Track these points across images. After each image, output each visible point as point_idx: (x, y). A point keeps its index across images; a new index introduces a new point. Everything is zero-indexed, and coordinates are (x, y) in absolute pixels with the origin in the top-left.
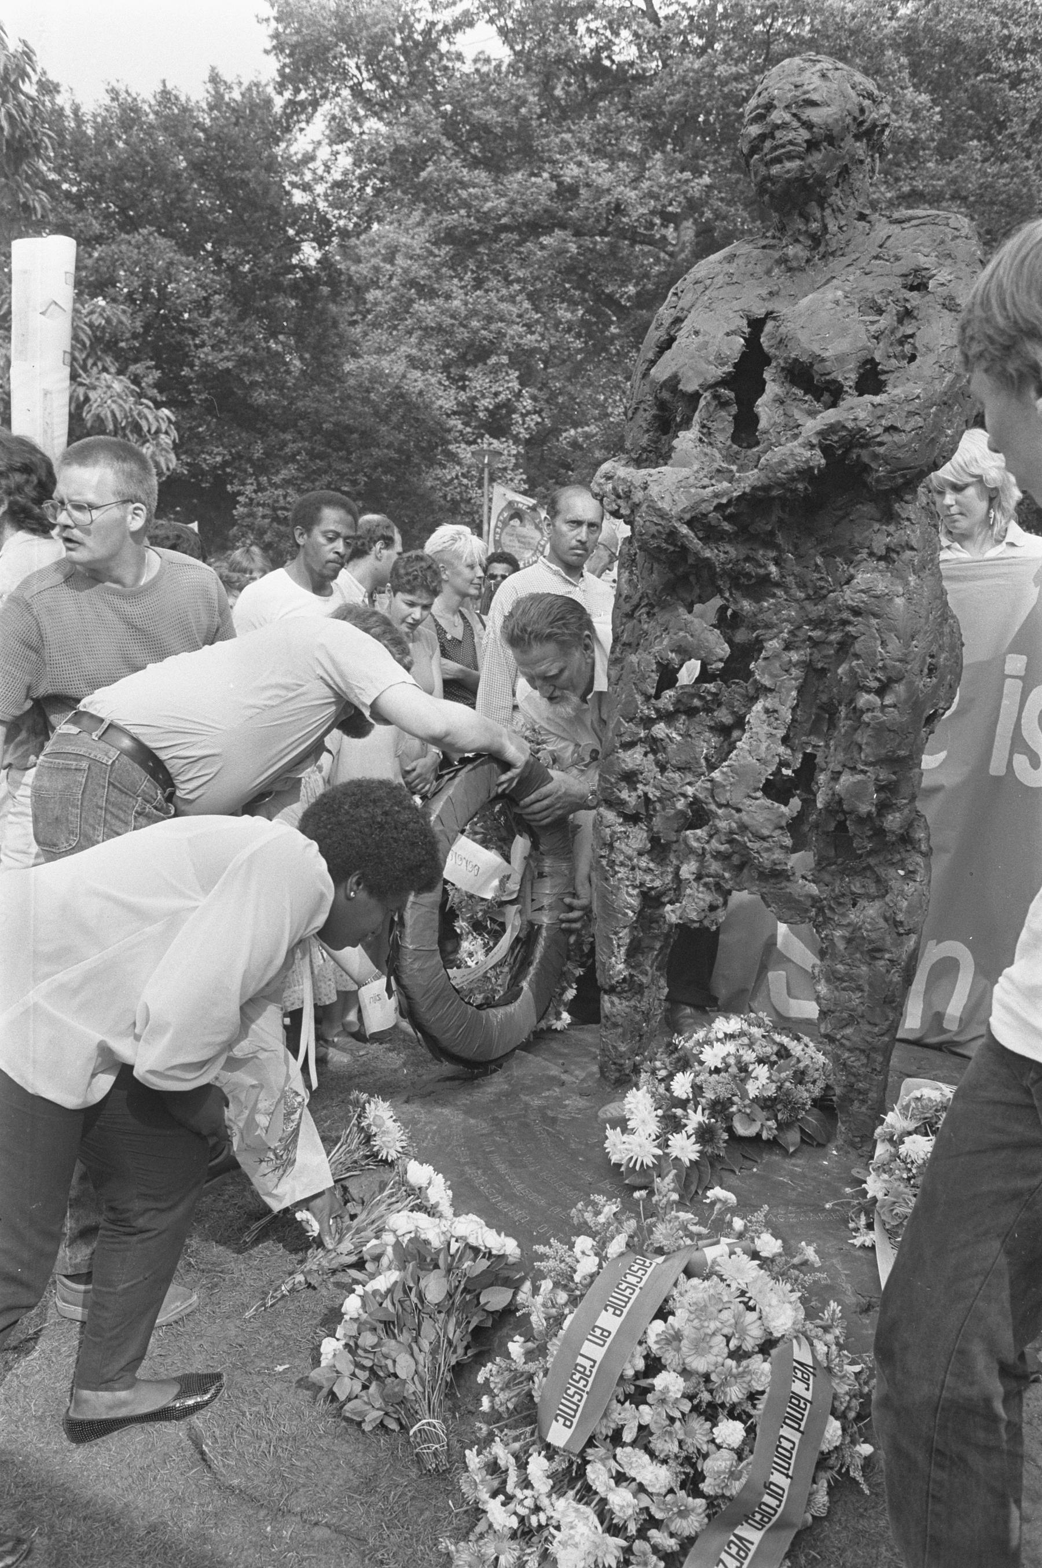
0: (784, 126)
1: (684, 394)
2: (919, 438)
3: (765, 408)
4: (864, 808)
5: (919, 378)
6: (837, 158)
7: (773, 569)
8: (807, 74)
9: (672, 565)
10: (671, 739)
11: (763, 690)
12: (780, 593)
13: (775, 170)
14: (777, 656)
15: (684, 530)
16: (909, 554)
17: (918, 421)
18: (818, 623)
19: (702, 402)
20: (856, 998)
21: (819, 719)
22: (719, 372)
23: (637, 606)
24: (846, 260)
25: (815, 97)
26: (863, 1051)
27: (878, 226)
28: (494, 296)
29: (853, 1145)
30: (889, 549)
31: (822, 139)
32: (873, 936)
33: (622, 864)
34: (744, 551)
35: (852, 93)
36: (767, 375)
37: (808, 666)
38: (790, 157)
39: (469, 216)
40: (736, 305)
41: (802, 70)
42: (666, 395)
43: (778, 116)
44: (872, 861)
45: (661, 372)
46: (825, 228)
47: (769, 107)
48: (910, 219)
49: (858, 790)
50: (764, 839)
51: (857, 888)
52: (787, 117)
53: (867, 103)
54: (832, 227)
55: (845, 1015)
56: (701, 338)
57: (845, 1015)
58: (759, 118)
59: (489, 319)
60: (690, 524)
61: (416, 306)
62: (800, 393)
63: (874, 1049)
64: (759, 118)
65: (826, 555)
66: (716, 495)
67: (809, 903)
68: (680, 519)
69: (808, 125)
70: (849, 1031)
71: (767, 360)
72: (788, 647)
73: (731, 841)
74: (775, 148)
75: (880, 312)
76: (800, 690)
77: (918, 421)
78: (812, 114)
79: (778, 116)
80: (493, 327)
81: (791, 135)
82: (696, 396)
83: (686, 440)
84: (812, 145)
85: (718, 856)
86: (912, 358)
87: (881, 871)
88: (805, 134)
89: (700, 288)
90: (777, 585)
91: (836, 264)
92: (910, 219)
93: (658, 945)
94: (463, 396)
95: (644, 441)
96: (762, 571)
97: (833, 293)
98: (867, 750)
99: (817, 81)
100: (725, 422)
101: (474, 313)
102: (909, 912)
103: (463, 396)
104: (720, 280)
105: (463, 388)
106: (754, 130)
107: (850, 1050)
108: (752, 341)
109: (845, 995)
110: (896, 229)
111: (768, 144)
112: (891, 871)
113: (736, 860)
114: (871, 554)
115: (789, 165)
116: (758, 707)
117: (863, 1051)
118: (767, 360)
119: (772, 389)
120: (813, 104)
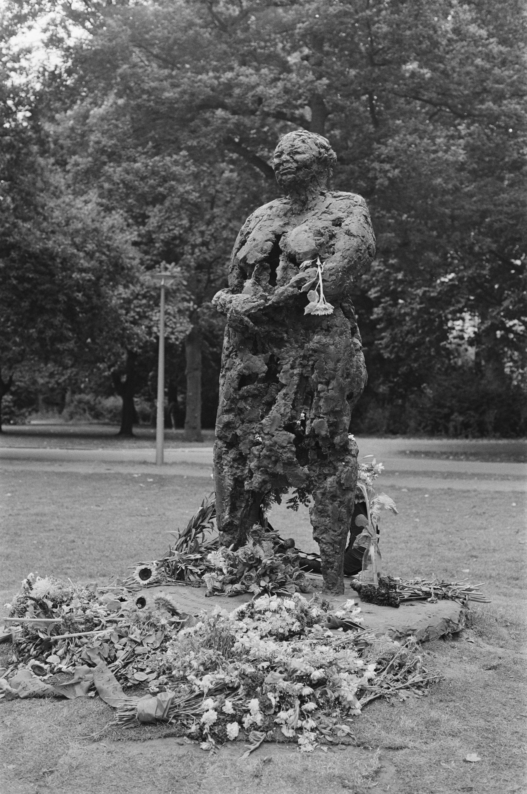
0: (287, 161)
1: (249, 265)
2: (334, 284)
3: (279, 271)
4: (323, 433)
5: (335, 261)
6: (310, 173)
7: (285, 335)
8: (296, 141)
9: (243, 333)
10: (247, 409)
11: (283, 386)
12: (288, 345)
13: (284, 178)
14: (288, 371)
15: (246, 319)
16: (335, 329)
17: (334, 277)
18: (304, 357)
19: (256, 268)
20: (327, 520)
21: (307, 398)
22: (261, 256)
23: (231, 352)
24: (313, 212)
25: (299, 150)
26: (331, 544)
27: (328, 198)
28: (166, 161)
29: (328, 588)
30: (328, 327)
31: (303, 166)
32: (332, 490)
33: (226, 465)
34: (272, 328)
35: (316, 148)
36: (281, 258)
37: (301, 375)
38: (290, 173)
39: (149, 101)
40: (271, 229)
41: (295, 139)
42: (241, 264)
43: (285, 157)
44: (332, 459)
45: (241, 255)
46: (307, 198)
47: (282, 153)
48: (339, 196)
49: (320, 426)
50: (284, 447)
51: (326, 471)
52: (288, 158)
53: (322, 150)
54: (310, 198)
55: (323, 528)
56: (256, 242)
57: (323, 528)
58: (279, 156)
59: (165, 180)
60: (248, 316)
61: (106, 168)
62: (292, 265)
63: (335, 542)
64: (279, 156)
65: (306, 329)
66: (258, 305)
67: (304, 477)
68: (244, 315)
69: (296, 161)
70: (324, 535)
71: (281, 252)
72: (292, 367)
73: (271, 450)
74: (284, 170)
75: (322, 235)
76: (298, 385)
77: (334, 277)
78: (298, 157)
79: (285, 157)
80: (167, 185)
81: (290, 165)
82: (253, 265)
83: (248, 283)
84: (298, 169)
85: (266, 456)
86: (333, 253)
87: (335, 463)
88: (295, 165)
89: (258, 219)
90: (287, 342)
91: (310, 214)
92: (339, 196)
93: (243, 505)
94: (143, 230)
95: (236, 282)
96: (280, 336)
97: (304, 227)
98: (323, 408)
99: (300, 144)
100: (266, 276)
101: (154, 173)
102: (347, 479)
103: (143, 230)
104: (265, 217)
105: (144, 224)
106: (276, 161)
107: (325, 544)
108: (276, 244)
109: (323, 519)
110: (334, 200)
111: (281, 167)
112: (339, 464)
113: (273, 459)
114: (322, 329)
115: (289, 176)
116: (281, 393)
117: (331, 544)
118: (281, 252)
119: (282, 264)
120: (299, 153)
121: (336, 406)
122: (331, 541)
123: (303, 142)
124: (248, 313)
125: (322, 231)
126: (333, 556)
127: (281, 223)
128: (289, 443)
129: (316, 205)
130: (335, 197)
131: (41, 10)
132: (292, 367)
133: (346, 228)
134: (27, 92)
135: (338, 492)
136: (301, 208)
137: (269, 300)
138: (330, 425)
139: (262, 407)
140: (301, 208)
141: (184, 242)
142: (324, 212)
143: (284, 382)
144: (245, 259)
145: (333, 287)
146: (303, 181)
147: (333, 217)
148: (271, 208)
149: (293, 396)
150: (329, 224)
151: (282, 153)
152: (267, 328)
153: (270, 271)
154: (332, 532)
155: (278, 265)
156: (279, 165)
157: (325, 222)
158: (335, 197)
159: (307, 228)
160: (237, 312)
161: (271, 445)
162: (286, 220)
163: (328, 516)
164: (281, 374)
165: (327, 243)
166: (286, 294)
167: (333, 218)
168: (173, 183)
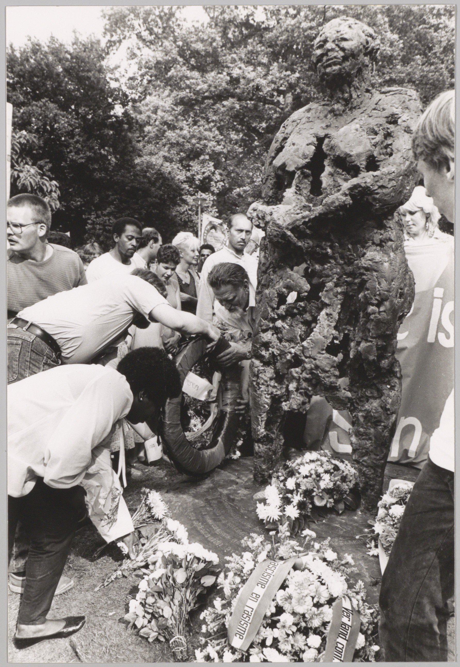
0: (332, 50)
1: (288, 172)
4: (371, 358)
6: (356, 64)
10: (284, 328)
11: (325, 305)
12: (332, 261)
13: (328, 70)
15: (289, 233)
17: (394, 183)
19: (297, 176)
20: (368, 443)
22: (302, 162)
24: (361, 111)
27: (375, 95)
31: (350, 55)
33: (263, 384)
36: (326, 163)
38: (335, 64)
40: (312, 131)
42: (280, 172)
43: (329, 45)
44: (375, 382)
45: (278, 162)
46: (351, 96)
47: (325, 41)
48: (389, 92)
49: (368, 350)
50: (327, 372)
52: (334, 46)
53: (369, 39)
54: (354, 96)
56: (295, 147)
57: (364, 451)
58: (321, 47)
59: (200, 139)
64: (321, 47)
66: (303, 217)
68: (287, 228)
69: (343, 49)
70: (365, 458)
71: (325, 156)
75: (376, 134)
77: (394, 183)
78: (345, 44)
79: (329, 45)
81: (335, 54)
83: (289, 193)
84: (345, 58)
85: (306, 380)
86: (391, 155)
88: (341, 54)
89: (295, 124)
91: (356, 112)
93: (279, 420)
94: (189, 174)
95: (270, 193)
97: (354, 125)
99: (347, 29)
101: (193, 136)
105: (189, 170)
106: (319, 52)
109: (364, 442)
110: (383, 96)
111: (325, 58)
112: (384, 386)
116: (323, 313)
118: (325, 156)
121: (387, 330)
122: (371, 464)
123: (350, 27)
124: (295, 229)
125: (376, 129)
126: (373, 479)
127: (324, 125)
128: (333, 366)
129: (361, 103)
130: (384, 93)
131: (124, 38)
132: (336, 285)
133: (405, 124)
134: (119, 92)
135: (383, 417)
136: (343, 108)
137: (313, 210)
138: (378, 349)
139: (300, 325)
140: (343, 108)
141: (211, 180)
142: (374, 109)
143: (327, 301)
144: (284, 166)
145: (393, 194)
146: (349, 74)
147: (386, 113)
148: (309, 110)
149: (337, 317)
150: (383, 121)
151: (325, 41)
152: (311, 243)
153: (311, 179)
154: (373, 456)
155: (323, 170)
156: (322, 55)
157: (376, 120)
158: (384, 93)
159: (358, 126)
160: (279, 226)
161: (312, 369)
162: (327, 122)
163: (370, 439)
164: (324, 293)
165: (382, 143)
166: (337, 204)
167: (387, 115)
168: (205, 141)
